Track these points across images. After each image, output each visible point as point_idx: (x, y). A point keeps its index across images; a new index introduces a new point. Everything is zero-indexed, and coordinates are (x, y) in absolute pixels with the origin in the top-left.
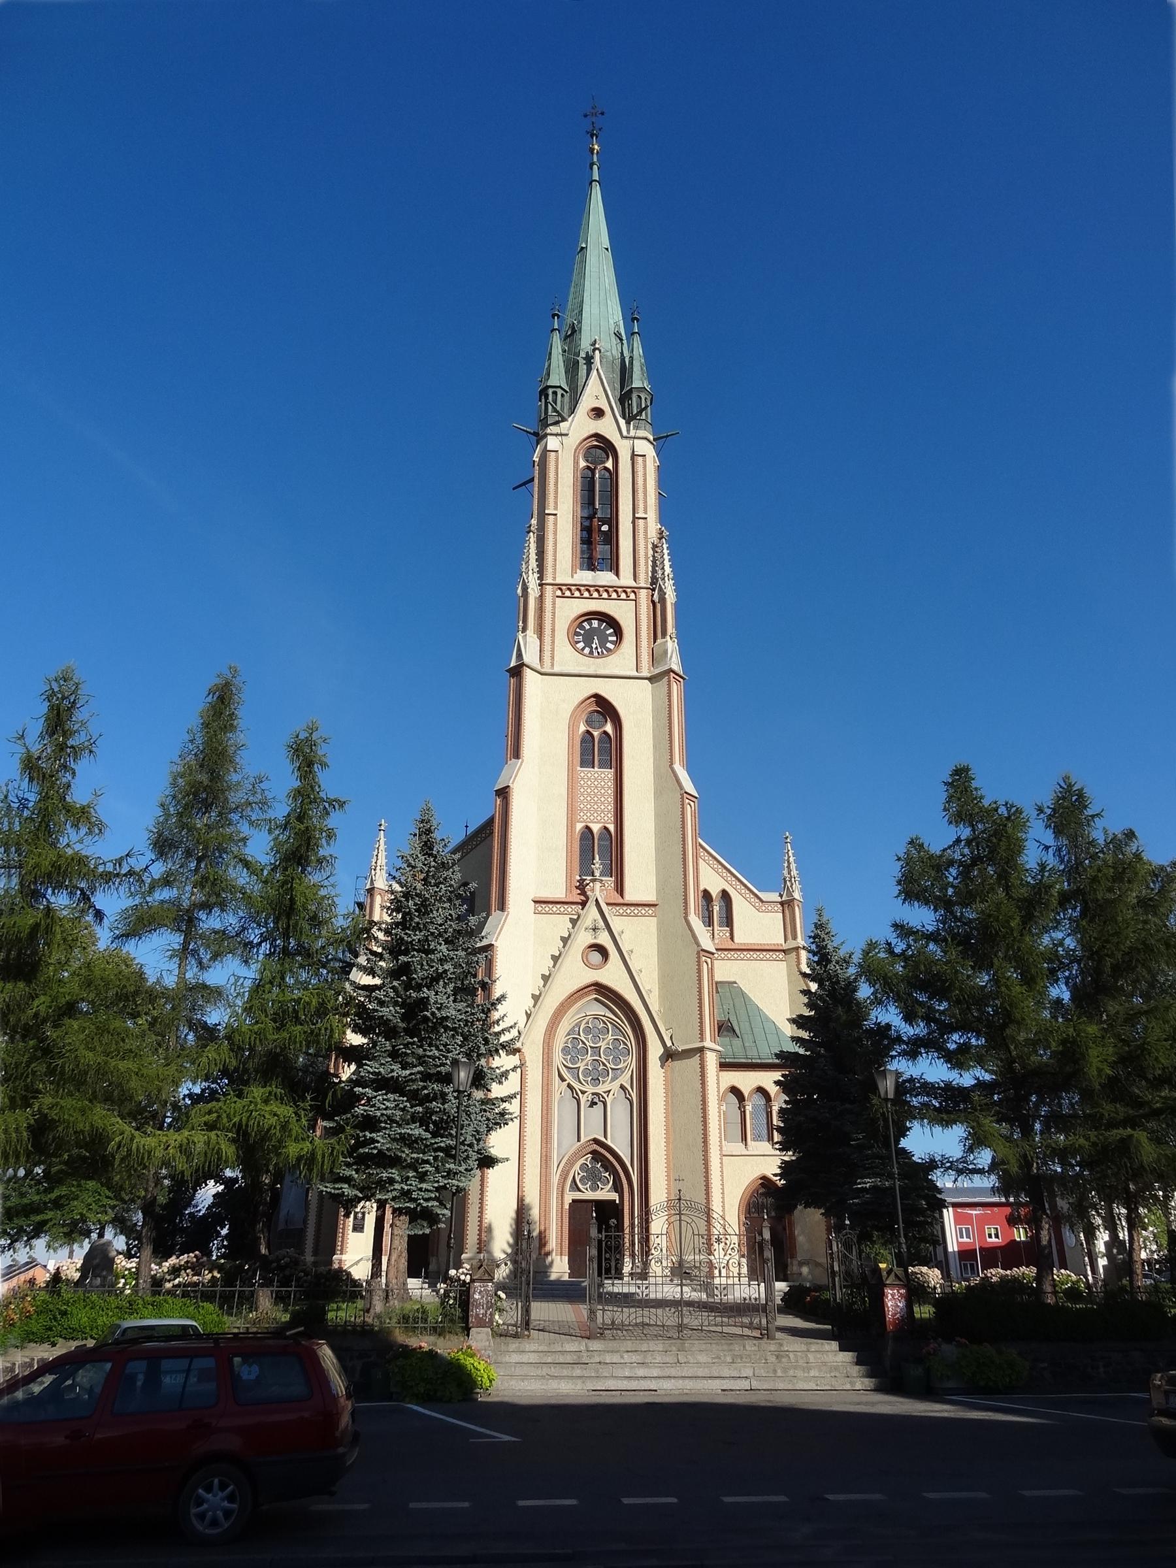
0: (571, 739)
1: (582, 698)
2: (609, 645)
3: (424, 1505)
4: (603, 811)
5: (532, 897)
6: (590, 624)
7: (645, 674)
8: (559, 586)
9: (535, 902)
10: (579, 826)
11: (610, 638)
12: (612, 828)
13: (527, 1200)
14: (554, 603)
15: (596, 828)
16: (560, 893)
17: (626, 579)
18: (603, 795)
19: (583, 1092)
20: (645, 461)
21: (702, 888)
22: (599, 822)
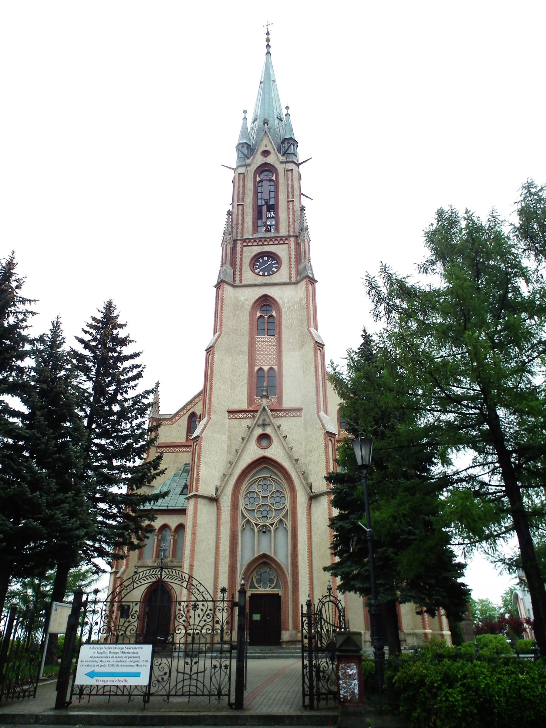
0: (251, 320)
1: (257, 297)
2: (274, 269)
3: (76, 713)
4: (270, 359)
5: (227, 409)
6: (263, 259)
7: (294, 280)
8: (244, 241)
9: (229, 412)
10: (256, 368)
11: (274, 266)
12: (275, 367)
13: (80, 337)
14: (242, 250)
15: (266, 368)
16: (244, 407)
17: (283, 232)
18: (270, 350)
19: (257, 525)
20: (292, 173)
21: (436, 618)
22: (268, 365)
